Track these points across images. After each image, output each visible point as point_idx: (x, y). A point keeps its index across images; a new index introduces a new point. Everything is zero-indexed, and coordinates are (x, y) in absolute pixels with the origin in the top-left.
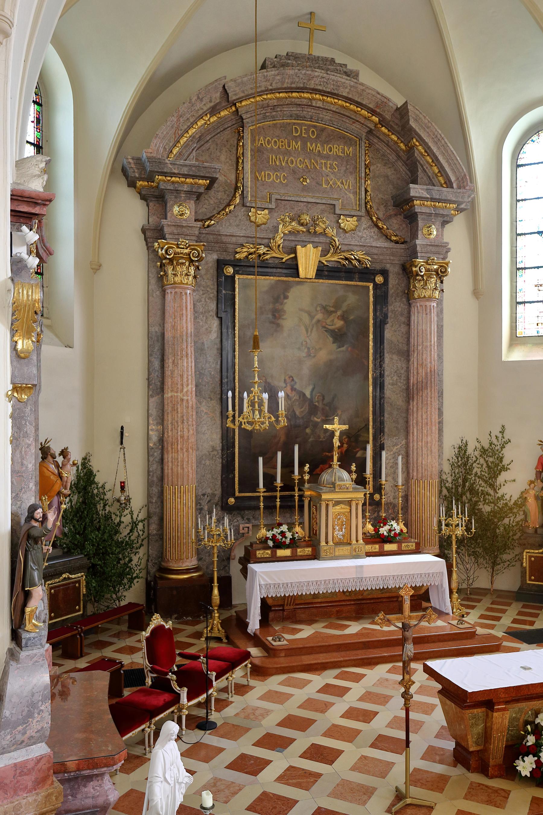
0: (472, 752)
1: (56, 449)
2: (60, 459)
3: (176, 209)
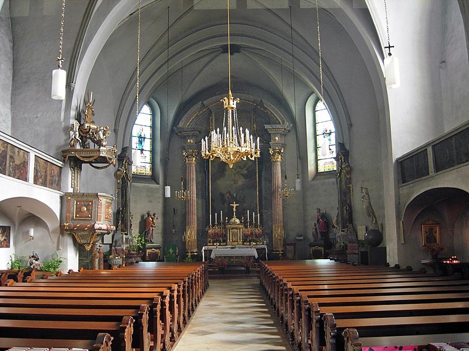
0: (80, 248)
1: (152, 214)
2: (153, 217)
3: (189, 141)
